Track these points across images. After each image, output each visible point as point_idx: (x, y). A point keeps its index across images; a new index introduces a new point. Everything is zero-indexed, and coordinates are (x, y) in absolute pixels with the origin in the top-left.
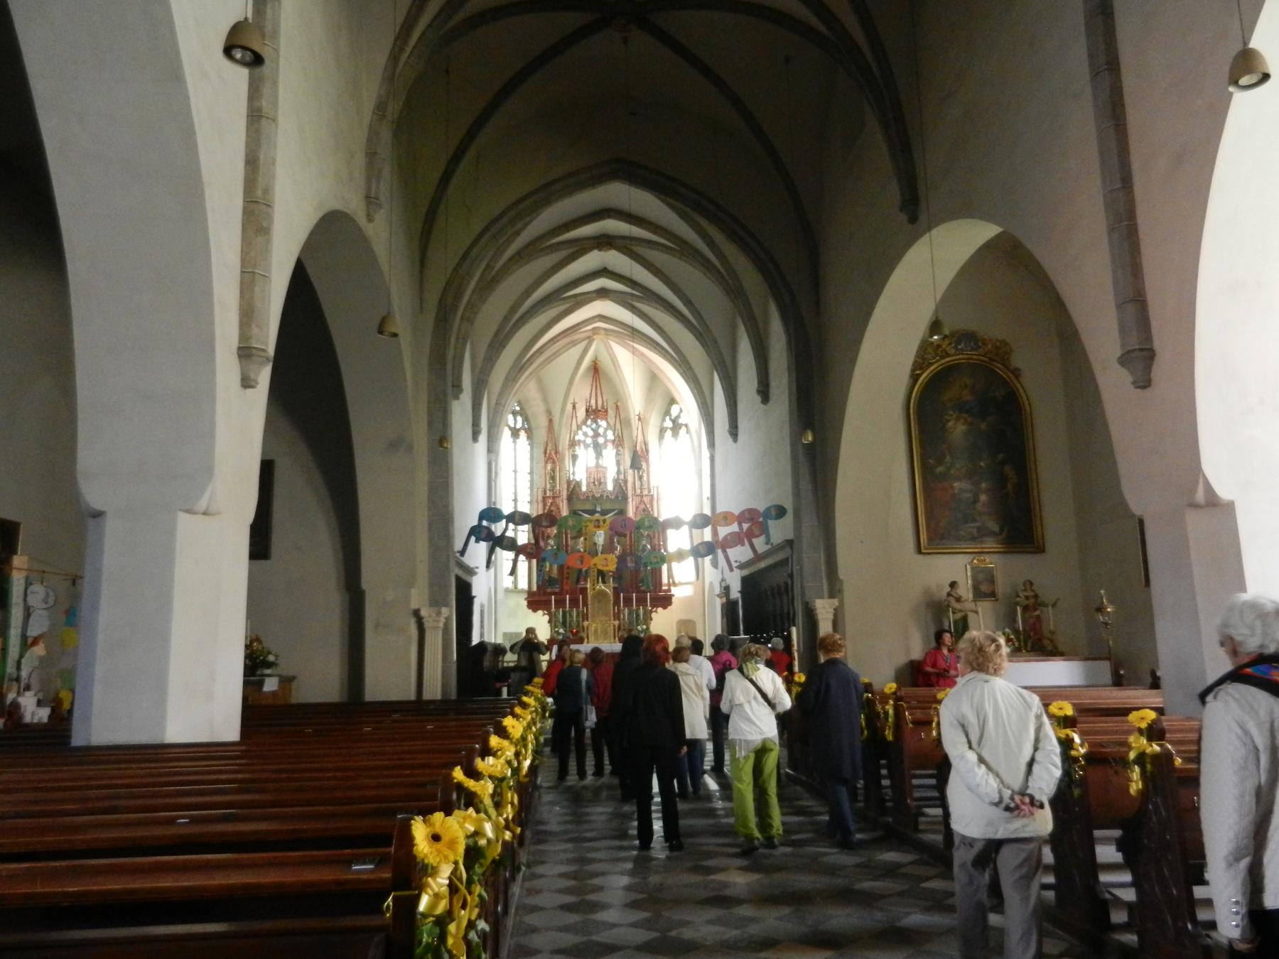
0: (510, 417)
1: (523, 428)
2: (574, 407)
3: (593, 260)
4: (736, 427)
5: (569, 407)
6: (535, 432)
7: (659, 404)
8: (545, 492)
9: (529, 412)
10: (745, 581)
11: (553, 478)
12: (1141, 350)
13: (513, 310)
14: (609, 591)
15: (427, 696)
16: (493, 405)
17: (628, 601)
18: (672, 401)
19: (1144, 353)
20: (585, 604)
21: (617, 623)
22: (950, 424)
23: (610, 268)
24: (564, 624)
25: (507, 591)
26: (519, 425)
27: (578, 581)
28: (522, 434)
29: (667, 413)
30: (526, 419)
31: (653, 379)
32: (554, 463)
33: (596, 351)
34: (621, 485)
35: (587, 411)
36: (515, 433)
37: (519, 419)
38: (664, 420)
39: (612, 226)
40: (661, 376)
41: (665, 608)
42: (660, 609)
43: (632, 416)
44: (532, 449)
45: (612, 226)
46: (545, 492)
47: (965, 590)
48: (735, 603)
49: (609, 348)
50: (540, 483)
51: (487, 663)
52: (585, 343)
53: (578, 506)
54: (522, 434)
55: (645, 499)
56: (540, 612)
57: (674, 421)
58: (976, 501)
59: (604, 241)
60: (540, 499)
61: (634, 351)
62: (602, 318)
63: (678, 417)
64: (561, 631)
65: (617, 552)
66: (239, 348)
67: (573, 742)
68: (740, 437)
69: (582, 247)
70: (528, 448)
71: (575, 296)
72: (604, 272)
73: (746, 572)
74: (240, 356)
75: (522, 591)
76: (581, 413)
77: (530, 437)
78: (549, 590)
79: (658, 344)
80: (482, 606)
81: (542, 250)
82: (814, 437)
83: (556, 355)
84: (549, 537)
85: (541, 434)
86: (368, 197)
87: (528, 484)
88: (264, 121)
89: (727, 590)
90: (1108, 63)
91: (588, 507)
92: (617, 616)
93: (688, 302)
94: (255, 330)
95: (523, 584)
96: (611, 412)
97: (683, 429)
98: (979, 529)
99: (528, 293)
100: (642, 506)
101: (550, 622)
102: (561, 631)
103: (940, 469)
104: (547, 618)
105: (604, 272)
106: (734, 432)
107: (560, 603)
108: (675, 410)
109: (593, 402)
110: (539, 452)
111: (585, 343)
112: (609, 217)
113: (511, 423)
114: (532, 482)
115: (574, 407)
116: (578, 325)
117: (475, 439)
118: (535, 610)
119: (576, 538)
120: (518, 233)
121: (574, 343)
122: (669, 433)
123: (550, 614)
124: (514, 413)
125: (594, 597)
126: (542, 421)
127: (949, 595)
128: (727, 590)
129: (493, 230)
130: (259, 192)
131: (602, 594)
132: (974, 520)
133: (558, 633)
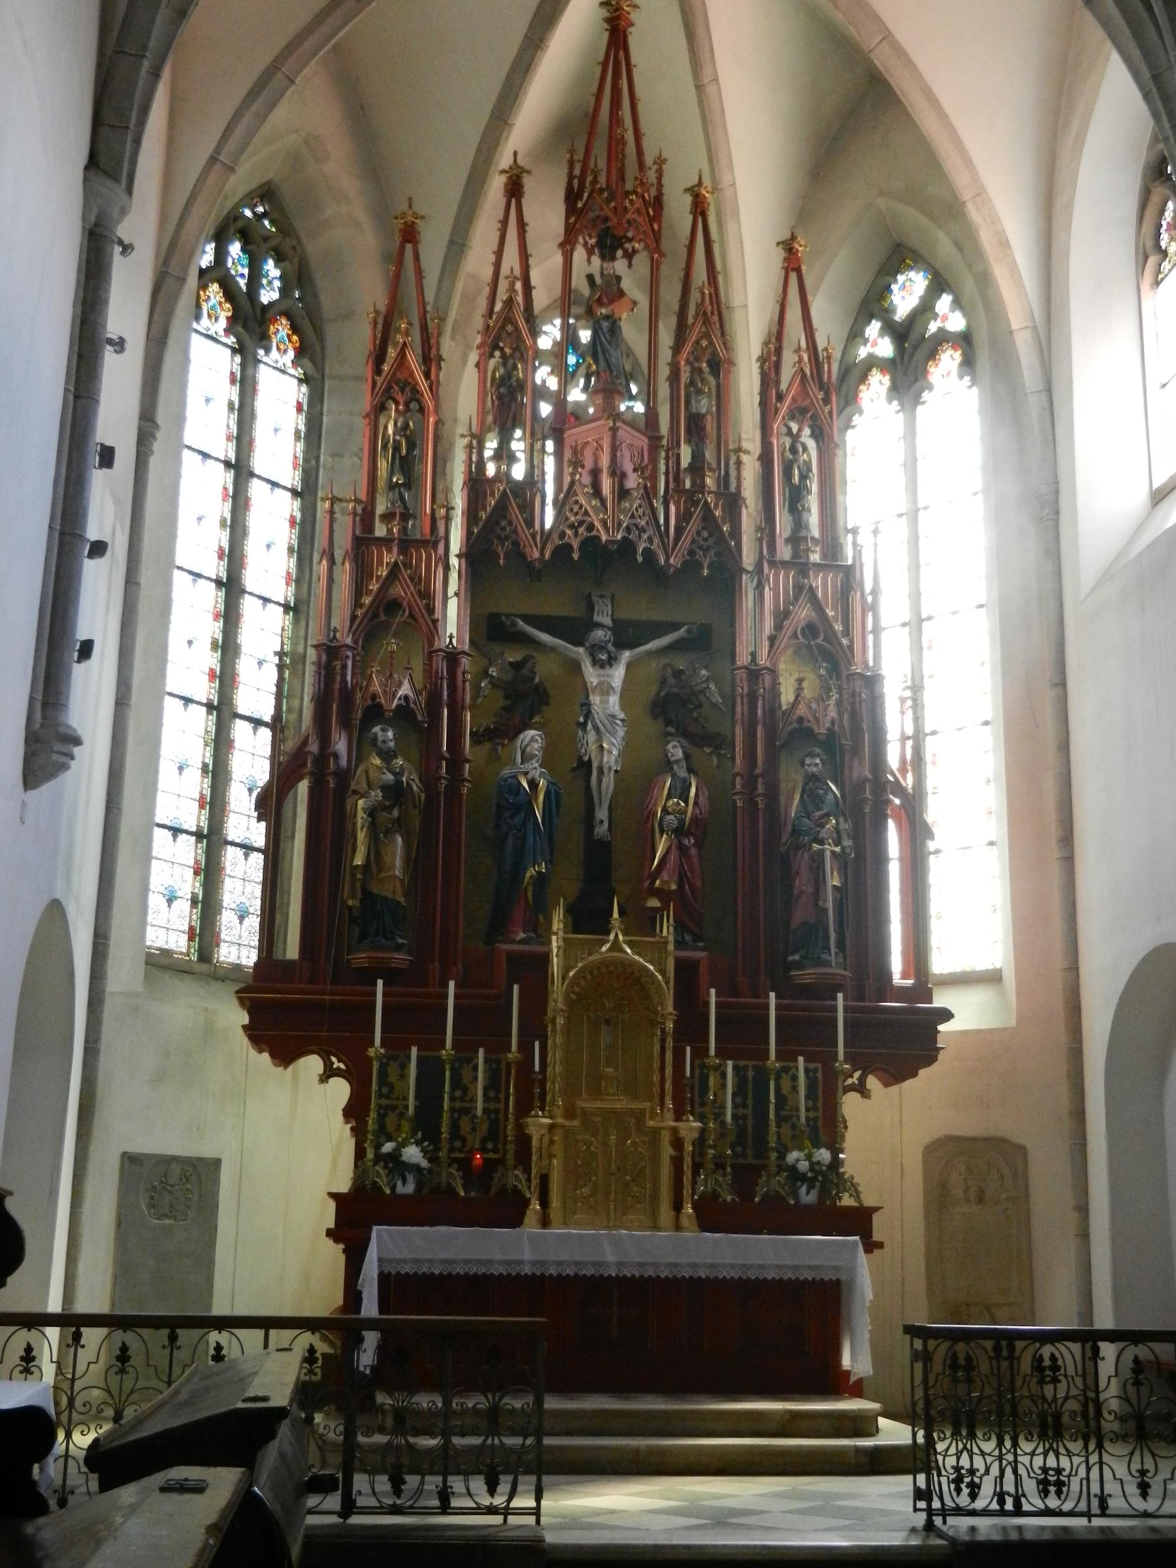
5: (497, 184)
6: (332, 334)
8: (366, 518)
9: (313, 248)
11: (406, 464)
14: (659, 973)
15: (533, 1478)
17: (742, 1033)
20: (535, 1028)
21: (691, 1127)
24: (426, 1126)
25: (160, 963)
27: (497, 927)
30: (298, 277)
44: (316, 398)
50: (347, 476)
53: (515, 601)
54: (281, 330)
56: (313, 1064)
57: (901, 333)
60: (344, 541)
64: (412, 1154)
65: (399, 1502)
67: (331, 795)
77: (310, 352)
78: (361, 958)
92: (689, 1096)
95: (239, 945)
100: (803, 613)
101: (354, 1112)
102: (412, 1154)
104: (340, 1090)
107: (413, 1021)
118: (285, 1055)
119: (500, 733)
123: (357, 1075)
125: (578, 1001)
126: (361, 288)
133: (394, 1162)
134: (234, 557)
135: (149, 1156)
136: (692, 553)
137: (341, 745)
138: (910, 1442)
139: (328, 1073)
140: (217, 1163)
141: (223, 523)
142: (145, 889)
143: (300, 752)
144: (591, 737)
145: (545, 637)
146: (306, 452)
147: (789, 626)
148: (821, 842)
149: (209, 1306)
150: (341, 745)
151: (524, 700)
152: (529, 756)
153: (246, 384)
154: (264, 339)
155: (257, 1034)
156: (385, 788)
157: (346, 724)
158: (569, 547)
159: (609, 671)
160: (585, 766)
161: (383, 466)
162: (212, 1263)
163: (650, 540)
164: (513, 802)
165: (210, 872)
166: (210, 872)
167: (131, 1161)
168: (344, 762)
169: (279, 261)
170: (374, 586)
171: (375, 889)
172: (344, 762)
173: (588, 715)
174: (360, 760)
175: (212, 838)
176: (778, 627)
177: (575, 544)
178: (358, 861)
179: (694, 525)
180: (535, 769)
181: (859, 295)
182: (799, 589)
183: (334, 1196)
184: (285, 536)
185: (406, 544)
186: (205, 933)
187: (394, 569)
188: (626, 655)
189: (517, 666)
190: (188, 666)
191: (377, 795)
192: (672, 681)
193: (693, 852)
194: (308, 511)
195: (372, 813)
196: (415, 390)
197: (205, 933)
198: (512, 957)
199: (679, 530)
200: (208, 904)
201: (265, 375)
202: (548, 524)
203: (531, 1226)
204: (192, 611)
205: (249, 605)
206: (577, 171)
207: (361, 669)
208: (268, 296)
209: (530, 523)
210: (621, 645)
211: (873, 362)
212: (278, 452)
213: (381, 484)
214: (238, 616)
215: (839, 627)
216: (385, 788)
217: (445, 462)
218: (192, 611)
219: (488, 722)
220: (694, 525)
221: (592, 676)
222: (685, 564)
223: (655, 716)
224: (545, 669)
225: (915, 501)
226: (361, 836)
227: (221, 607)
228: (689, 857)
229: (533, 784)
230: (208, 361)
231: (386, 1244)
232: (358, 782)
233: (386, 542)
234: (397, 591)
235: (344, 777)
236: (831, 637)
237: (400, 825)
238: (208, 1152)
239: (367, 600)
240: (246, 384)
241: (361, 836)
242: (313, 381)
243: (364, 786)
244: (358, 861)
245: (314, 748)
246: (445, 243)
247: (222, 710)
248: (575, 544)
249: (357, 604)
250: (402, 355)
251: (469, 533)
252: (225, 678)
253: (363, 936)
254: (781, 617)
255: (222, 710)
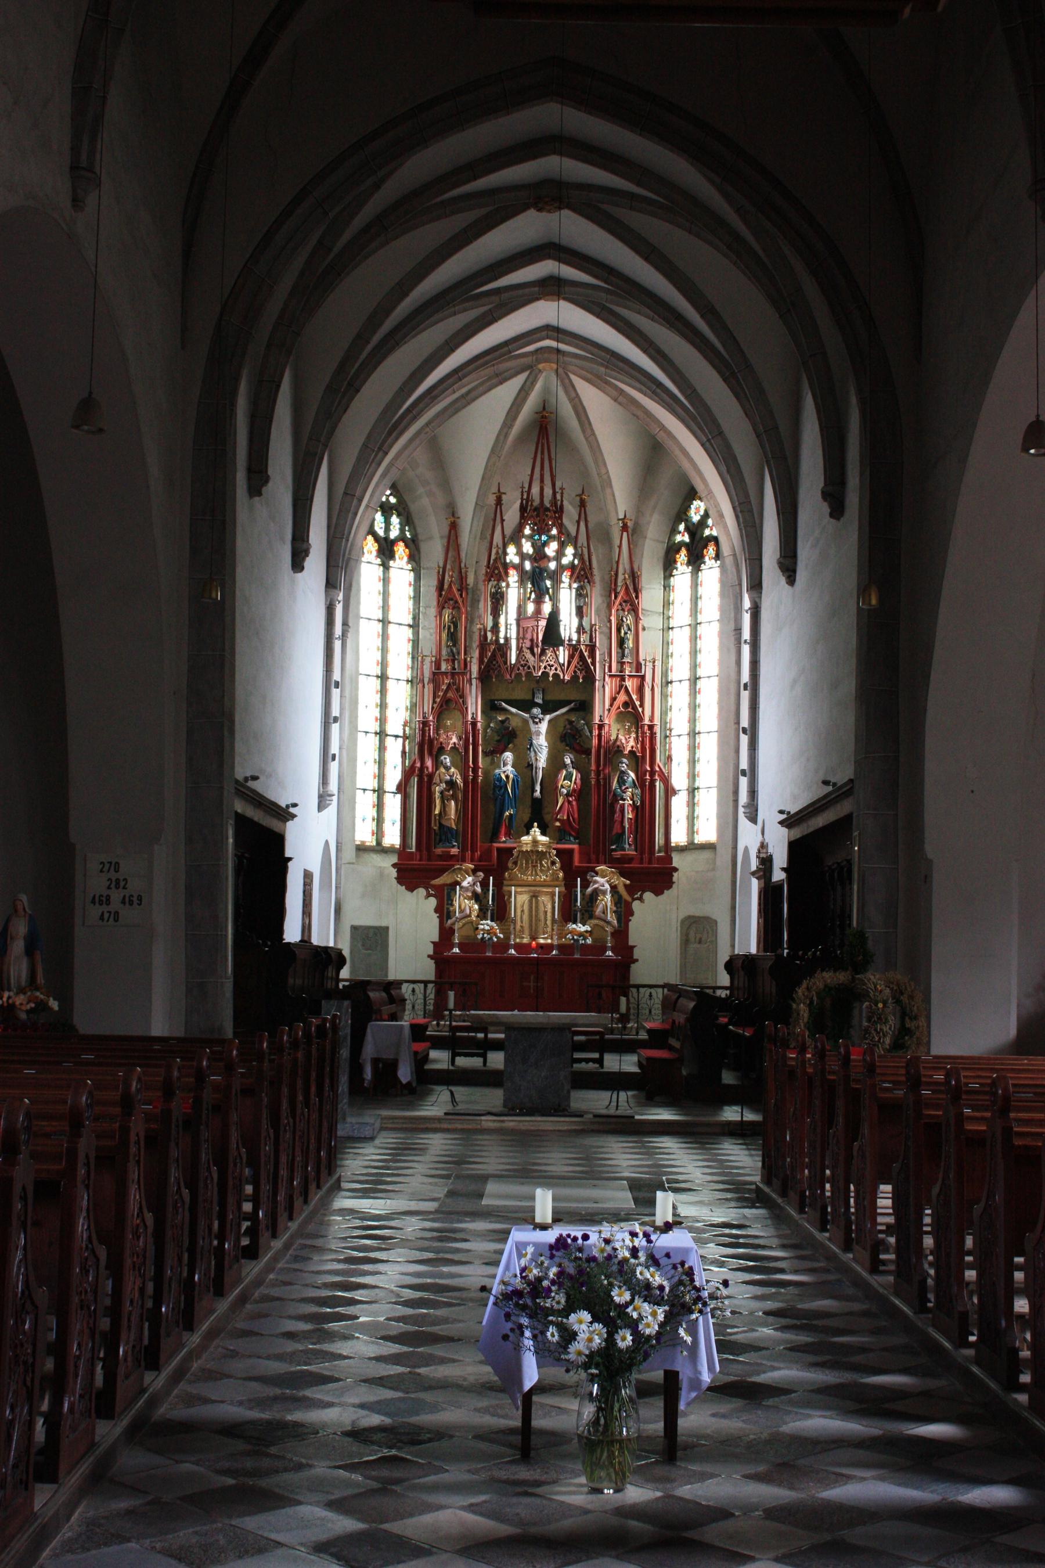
0: (379, 517)
1: (402, 538)
3: (526, 227)
4: (794, 556)
6: (423, 547)
7: (664, 496)
8: (438, 665)
9: (413, 507)
10: (794, 848)
16: (340, 489)
18: (692, 494)
26: (394, 533)
28: (400, 550)
29: (682, 515)
30: (407, 520)
31: (653, 452)
32: (456, 607)
33: (546, 390)
34: (583, 659)
35: (523, 509)
36: (386, 550)
37: (395, 520)
38: (674, 531)
40: (669, 444)
41: (658, 892)
42: (648, 896)
43: (613, 521)
46: (438, 665)
48: (779, 886)
49: (570, 389)
50: (428, 645)
51: (295, 980)
55: (629, 684)
57: (694, 530)
59: (549, 195)
61: (619, 397)
63: (702, 523)
68: (801, 575)
70: (411, 576)
71: (498, 291)
73: (797, 833)
76: (512, 515)
77: (414, 558)
79: (660, 385)
80: (308, 876)
82: (881, 600)
83: (468, 399)
84: (441, 750)
85: (434, 551)
86: (74, 168)
87: (409, 647)
89: (766, 862)
91: (520, 694)
93: (708, 312)
95: (392, 837)
96: (570, 511)
97: (711, 550)
99: (403, 289)
106: (789, 568)
108: (696, 510)
109: (535, 490)
110: (429, 585)
111: (521, 379)
113: (379, 528)
114: (415, 642)
116: (506, 343)
117: (298, 565)
118: (411, 888)
119: (494, 752)
120: (377, 186)
121: (501, 379)
122: (682, 556)
124: (387, 510)
128: (766, 862)
134: (384, 664)
135: (361, 927)
136: (575, 672)
137: (429, 763)
139: (429, 895)
140: (387, 928)
141: (376, 719)
142: (354, 817)
143: (412, 767)
144: (532, 754)
145: (514, 710)
146: (414, 605)
147: (616, 704)
148: (624, 800)
149: (386, 975)
150: (429, 763)
152: (507, 766)
153: (386, 581)
154: (391, 556)
155: (400, 880)
156: (447, 783)
157: (430, 754)
158: (520, 674)
159: (540, 725)
160: (530, 766)
161: (444, 636)
162: (387, 968)
163: (556, 669)
164: (499, 785)
165: (380, 806)
166: (380, 806)
167: (354, 929)
168: (430, 770)
169: (398, 516)
170: (441, 694)
171: (444, 822)
172: (430, 770)
173: (531, 744)
174: (437, 769)
176: (611, 705)
177: (523, 674)
178: (437, 812)
179: (575, 662)
180: (509, 768)
181: (676, 510)
182: (621, 686)
183: (433, 943)
186: (379, 833)
187: (449, 686)
188: (548, 717)
189: (502, 722)
190: (367, 718)
191: (444, 785)
192: (568, 727)
193: (574, 803)
194: (416, 634)
195: (442, 793)
196: (456, 602)
197: (379, 833)
198: (499, 850)
199: (569, 663)
201: (393, 573)
202: (513, 661)
204: (368, 691)
206: (525, 497)
207: (437, 729)
208: (394, 533)
209: (506, 663)
210: (545, 712)
211: (682, 544)
212: (402, 608)
213: (443, 643)
214: (383, 804)
215: (638, 703)
216: (447, 783)
218: (368, 691)
220: (575, 662)
221: (533, 728)
222: (572, 677)
223: (562, 741)
224: (514, 723)
225: (696, 619)
226: (438, 801)
227: (379, 688)
228: (572, 806)
229: (507, 777)
232: (436, 779)
233: (445, 673)
234: (450, 694)
235: (431, 776)
236: (634, 707)
237: (454, 797)
238: (384, 924)
239: (438, 700)
240: (386, 581)
241: (438, 801)
242: (417, 571)
243: (438, 781)
244: (437, 812)
245: (418, 765)
246: (474, 504)
247: (382, 734)
248: (523, 674)
249: (434, 702)
250: (450, 586)
251: (480, 668)
252: (382, 720)
253: (440, 841)
254: (613, 699)
255: (382, 734)
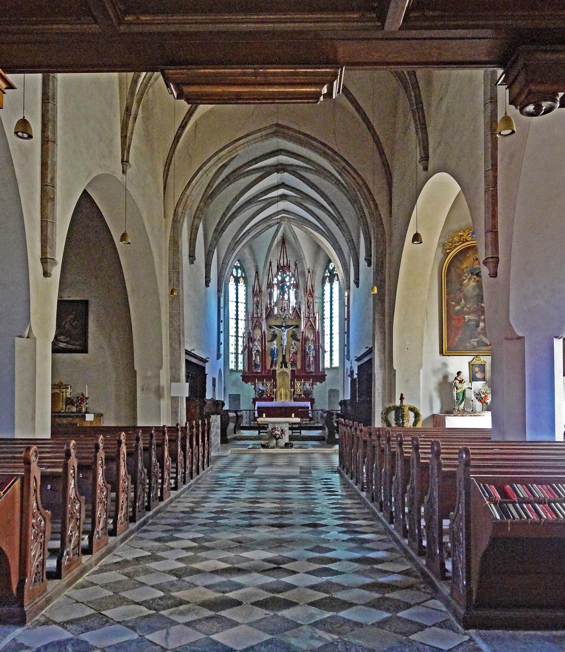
2: (270, 265)
3: (274, 179)
12: (492, 258)
13: (228, 209)
18: (330, 261)
19: (494, 259)
22: (465, 282)
23: (287, 183)
28: (241, 280)
30: (243, 271)
33: (285, 229)
35: (278, 267)
37: (239, 271)
38: (325, 272)
39: (283, 159)
42: (318, 383)
44: (247, 289)
45: (283, 159)
47: (465, 375)
48: (355, 380)
52: (276, 226)
54: (241, 280)
57: (331, 272)
58: (478, 326)
59: (280, 168)
62: (284, 211)
66: (41, 259)
69: (267, 172)
72: (282, 185)
74: (42, 263)
75: (241, 371)
76: (275, 269)
77: (246, 282)
81: (241, 175)
85: (252, 280)
88: (50, 143)
90: (491, 98)
94: (49, 249)
95: (241, 367)
98: (478, 342)
103: (458, 308)
105: (282, 185)
109: (282, 261)
111: (276, 226)
112: (281, 154)
113: (235, 274)
115: (270, 265)
116: (271, 215)
121: (270, 226)
124: (237, 268)
127: (456, 379)
129: (205, 168)
130: (49, 180)
131: (284, 373)
132: (476, 338)
138: (490, 357)
151: (274, 336)
175: (237, 354)
180: (275, 346)
184: (244, 310)
185: (258, 318)
186: (237, 366)
194: (247, 306)
197: (237, 366)
200: (237, 362)
203: (274, 402)
205: (239, 321)
211: (327, 276)
217: (330, 162)
219: (269, 339)
224: (277, 332)
230: (232, 286)
231: (258, 404)
232: (253, 350)
234: (257, 324)
235: (252, 349)
255: (237, 336)
